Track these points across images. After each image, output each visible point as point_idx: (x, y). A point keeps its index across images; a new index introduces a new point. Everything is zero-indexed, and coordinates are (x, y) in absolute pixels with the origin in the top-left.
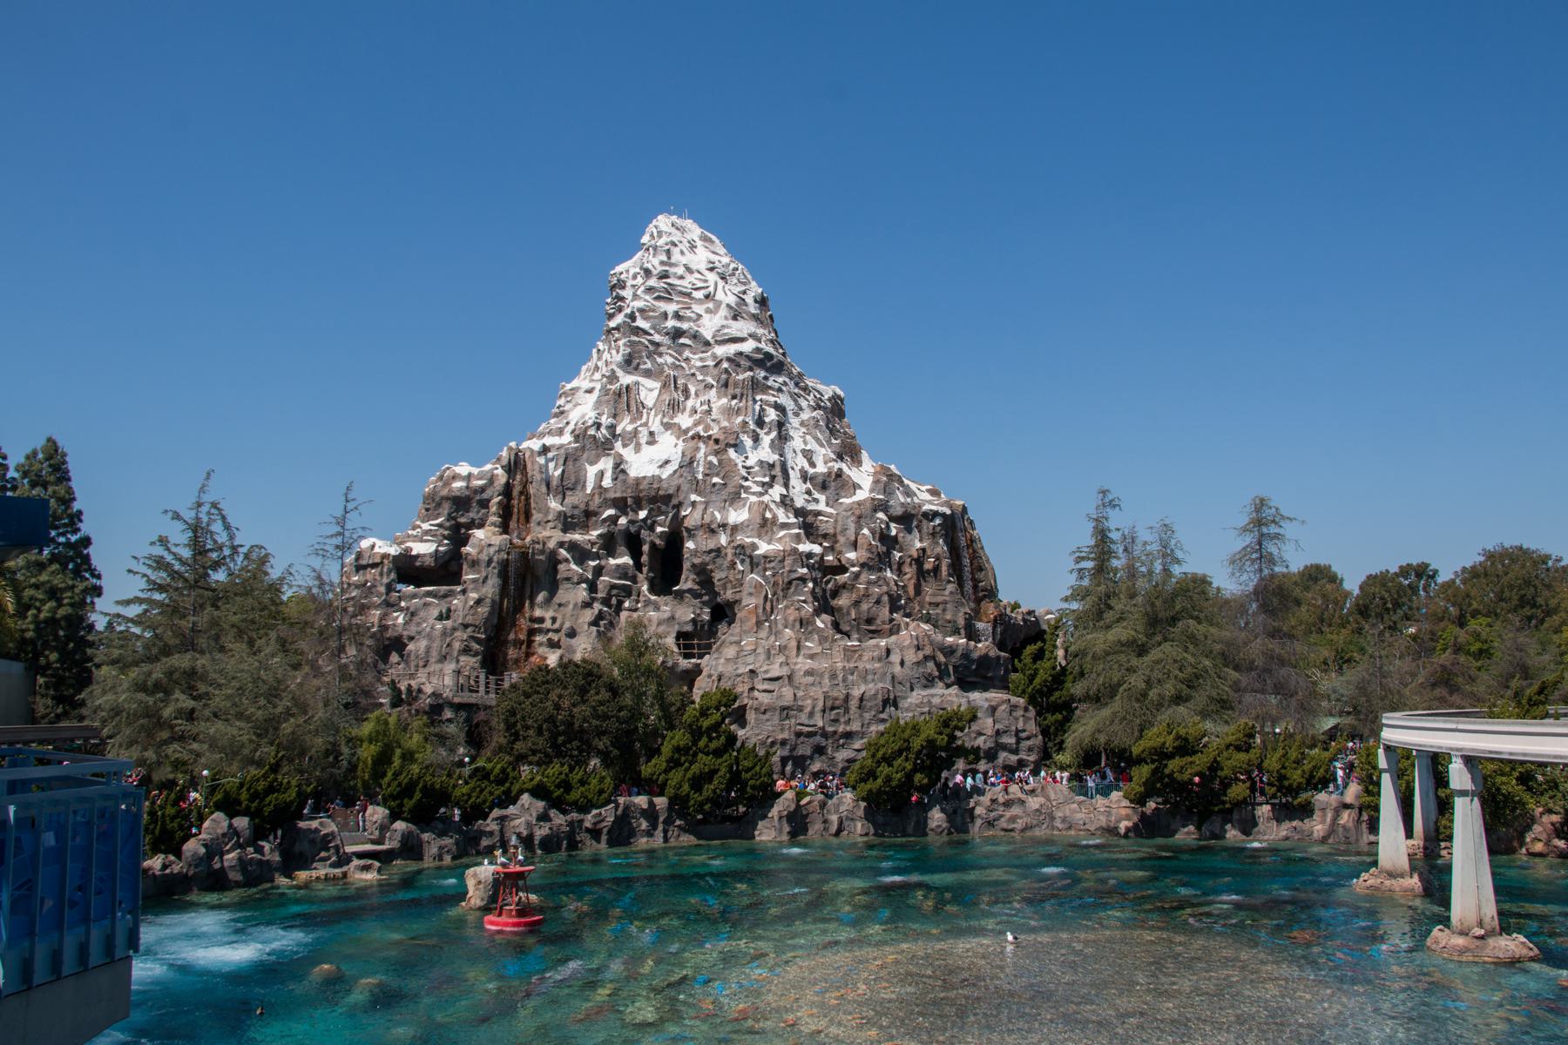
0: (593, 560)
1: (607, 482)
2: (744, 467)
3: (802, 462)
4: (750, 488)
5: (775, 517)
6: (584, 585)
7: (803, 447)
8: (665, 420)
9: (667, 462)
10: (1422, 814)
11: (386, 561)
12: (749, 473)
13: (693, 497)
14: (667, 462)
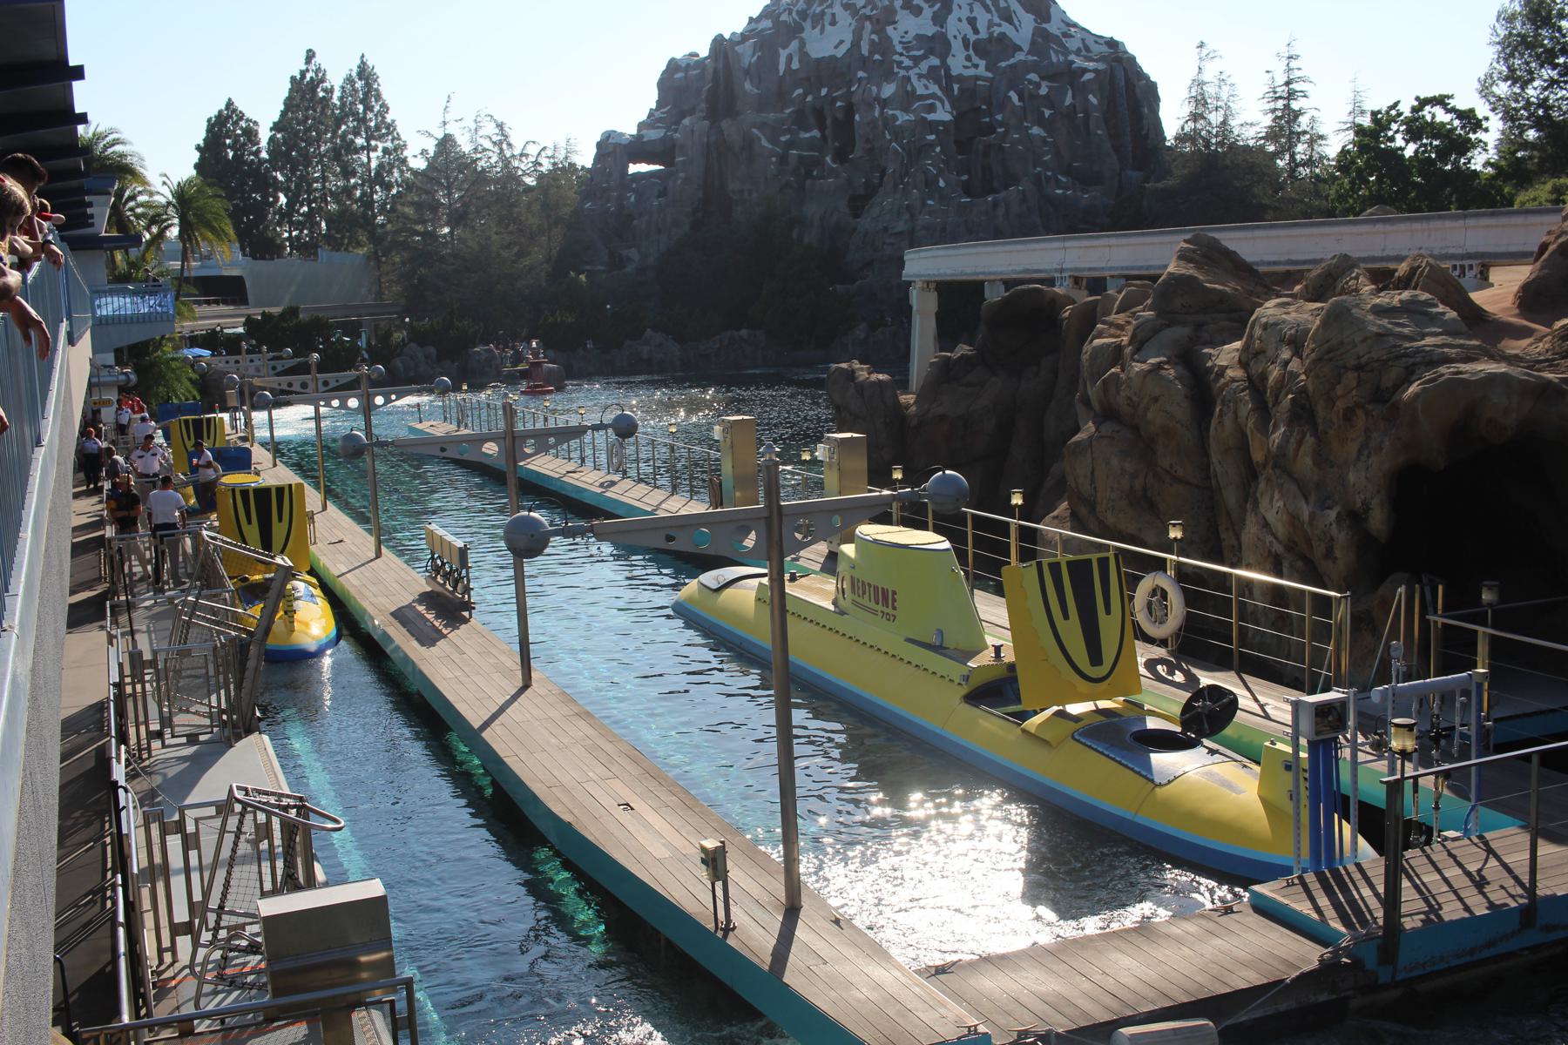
1: (795, 65)
2: (900, 42)
5: (914, 90)
6: (774, 159)
7: (969, 15)
9: (841, 42)
12: (904, 48)
13: (861, 74)
14: (841, 42)
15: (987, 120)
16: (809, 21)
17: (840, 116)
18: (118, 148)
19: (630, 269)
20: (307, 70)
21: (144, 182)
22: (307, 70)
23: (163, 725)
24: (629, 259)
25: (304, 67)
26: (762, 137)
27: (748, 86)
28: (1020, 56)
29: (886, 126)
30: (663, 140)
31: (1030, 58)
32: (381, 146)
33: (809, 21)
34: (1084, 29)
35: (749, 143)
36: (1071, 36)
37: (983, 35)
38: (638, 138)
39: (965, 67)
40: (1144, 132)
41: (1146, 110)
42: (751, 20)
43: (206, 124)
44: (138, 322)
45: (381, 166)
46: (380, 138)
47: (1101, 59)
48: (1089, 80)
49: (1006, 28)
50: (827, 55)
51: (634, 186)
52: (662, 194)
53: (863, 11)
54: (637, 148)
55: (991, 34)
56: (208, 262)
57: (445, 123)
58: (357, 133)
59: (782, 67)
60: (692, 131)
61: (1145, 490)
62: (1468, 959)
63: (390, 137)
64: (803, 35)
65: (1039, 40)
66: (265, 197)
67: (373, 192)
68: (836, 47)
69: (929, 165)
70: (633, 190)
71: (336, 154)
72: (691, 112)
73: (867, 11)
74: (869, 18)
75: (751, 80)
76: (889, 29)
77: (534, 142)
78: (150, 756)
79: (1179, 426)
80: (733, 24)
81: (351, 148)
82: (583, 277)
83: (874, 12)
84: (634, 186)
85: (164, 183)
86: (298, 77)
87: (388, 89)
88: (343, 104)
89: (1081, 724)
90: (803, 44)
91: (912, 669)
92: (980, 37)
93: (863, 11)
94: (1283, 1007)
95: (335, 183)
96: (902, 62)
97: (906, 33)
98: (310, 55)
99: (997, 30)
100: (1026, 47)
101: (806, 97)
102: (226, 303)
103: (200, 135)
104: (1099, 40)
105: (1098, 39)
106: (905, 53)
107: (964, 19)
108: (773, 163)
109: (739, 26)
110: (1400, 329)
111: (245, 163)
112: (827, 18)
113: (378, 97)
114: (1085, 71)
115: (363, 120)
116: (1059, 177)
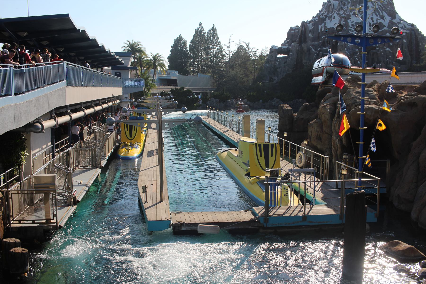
0: (319, 48)
1: (323, 30)
2: (351, 24)
3: (370, 21)
4: (351, 29)
6: (315, 55)
8: (337, 13)
9: (336, 24)
10: (33, 226)
11: (275, 51)
12: (352, 26)
14: (336, 24)
15: (374, 46)
16: (328, 18)
17: (334, 43)
18: (140, 46)
19: (274, 82)
20: (199, 28)
21: (145, 55)
22: (199, 28)
23: (78, 164)
24: (275, 79)
25: (199, 27)
26: (312, 48)
27: (310, 35)
28: (385, 28)
29: (345, 47)
30: (288, 48)
31: (388, 29)
32: (217, 48)
33: (328, 18)
34: (405, 21)
35: (309, 50)
36: (400, 23)
37: (375, 22)
38: (281, 48)
39: (369, 31)
40: (419, 50)
41: (420, 44)
42: (313, 17)
43: (174, 41)
44: (135, 88)
45: (216, 53)
46: (216, 46)
47: (408, 30)
48: (404, 35)
49: (382, 21)
50: (331, 27)
51: (279, 60)
52: (285, 63)
53: (342, 15)
54: (280, 51)
55: (377, 22)
56: (168, 75)
57: (229, 42)
58: (210, 44)
59: (319, 30)
60: (294, 46)
61: (320, 135)
62: (288, 225)
63: (219, 46)
64: (326, 22)
65: (391, 24)
66: (187, 60)
67: (214, 59)
68: (334, 25)
69: (356, 57)
70: (278, 61)
71: (205, 50)
72: (295, 41)
73: (343, 16)
74: (343, 17)
75: (311, 33)
76: (349, 21)
77: (255, 48)
78: (75, 170)
79: (327, 120)
80: (308, 18)
81: (209, 48)
82: (261, 83)
83: (345, 16)
84: (279, 60)
85: (151, 55)
86: (197, 29)
87: (219, 33)
88: (208, 37)
89: (260, 180)
90: (325, 24)
91: (242, 168)
92: (374, 23)
93: (342, 15)
94: (240, 227)
95: (204, 57)
96: (351, 29)
97: (353, 21)
98: (200, 24)
99: (379, 21)
100: (387, 26)
101: (325, 38)
102: (171, 85)
103: (172, 43)
104: (409, 24)
105: (408, 24)
106: (352, 27)
107: (370, 18)
108: (315, 56)
109: (310, 19)
110: (359, 97)
111: (183, 51)
112: (333, 17)
113: (217, 35)
114: (403, 33)
115: (212, 41)
116: (393, 62)
